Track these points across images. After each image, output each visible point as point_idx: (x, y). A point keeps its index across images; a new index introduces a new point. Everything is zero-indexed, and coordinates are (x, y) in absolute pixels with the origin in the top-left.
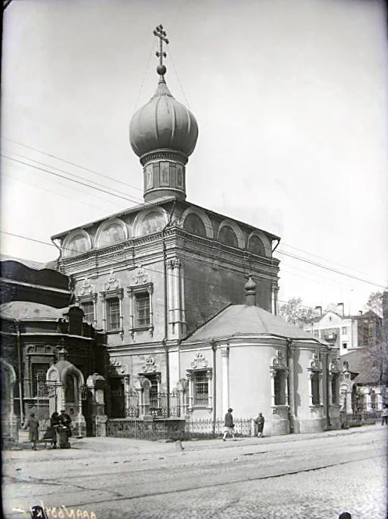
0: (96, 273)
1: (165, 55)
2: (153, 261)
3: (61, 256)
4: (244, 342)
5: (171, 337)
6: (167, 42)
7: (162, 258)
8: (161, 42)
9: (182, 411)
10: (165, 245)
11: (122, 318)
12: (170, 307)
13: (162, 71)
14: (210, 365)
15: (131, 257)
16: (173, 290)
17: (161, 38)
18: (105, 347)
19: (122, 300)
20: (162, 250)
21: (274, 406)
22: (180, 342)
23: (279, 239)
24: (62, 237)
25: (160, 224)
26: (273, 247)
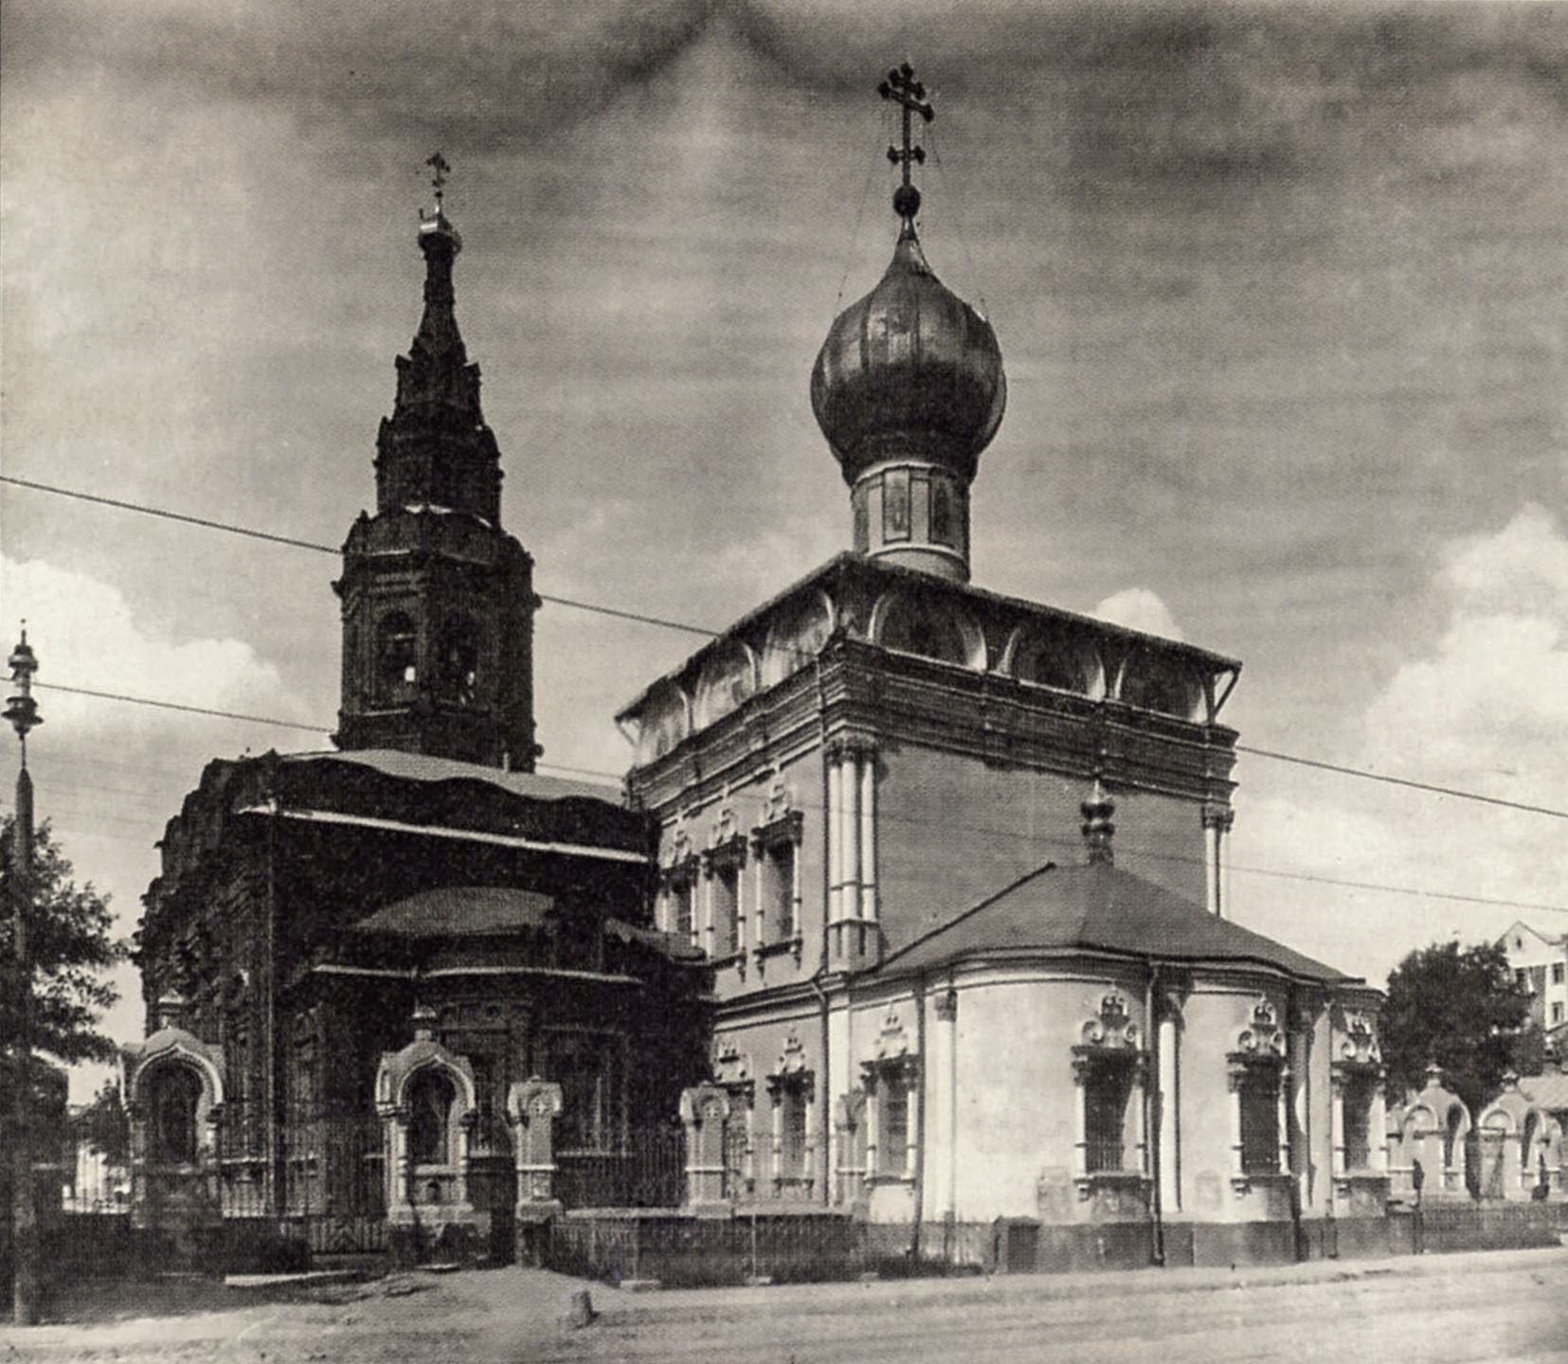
0: (695, 798)
1: (919, 155)
4: (1033, 967)
5: (833, 968)
6: (928, 114)
8: (906, 119)
9: (846, 1189)
11: (743, 919)
13: (907, 203)
14: (913, 1050)
15: (759, 745)
17: (908, 107)
18: (707, 1004)
23: (1235, 668)
24: (634, 712)
25: (819, 635)
26: (1218, 693)
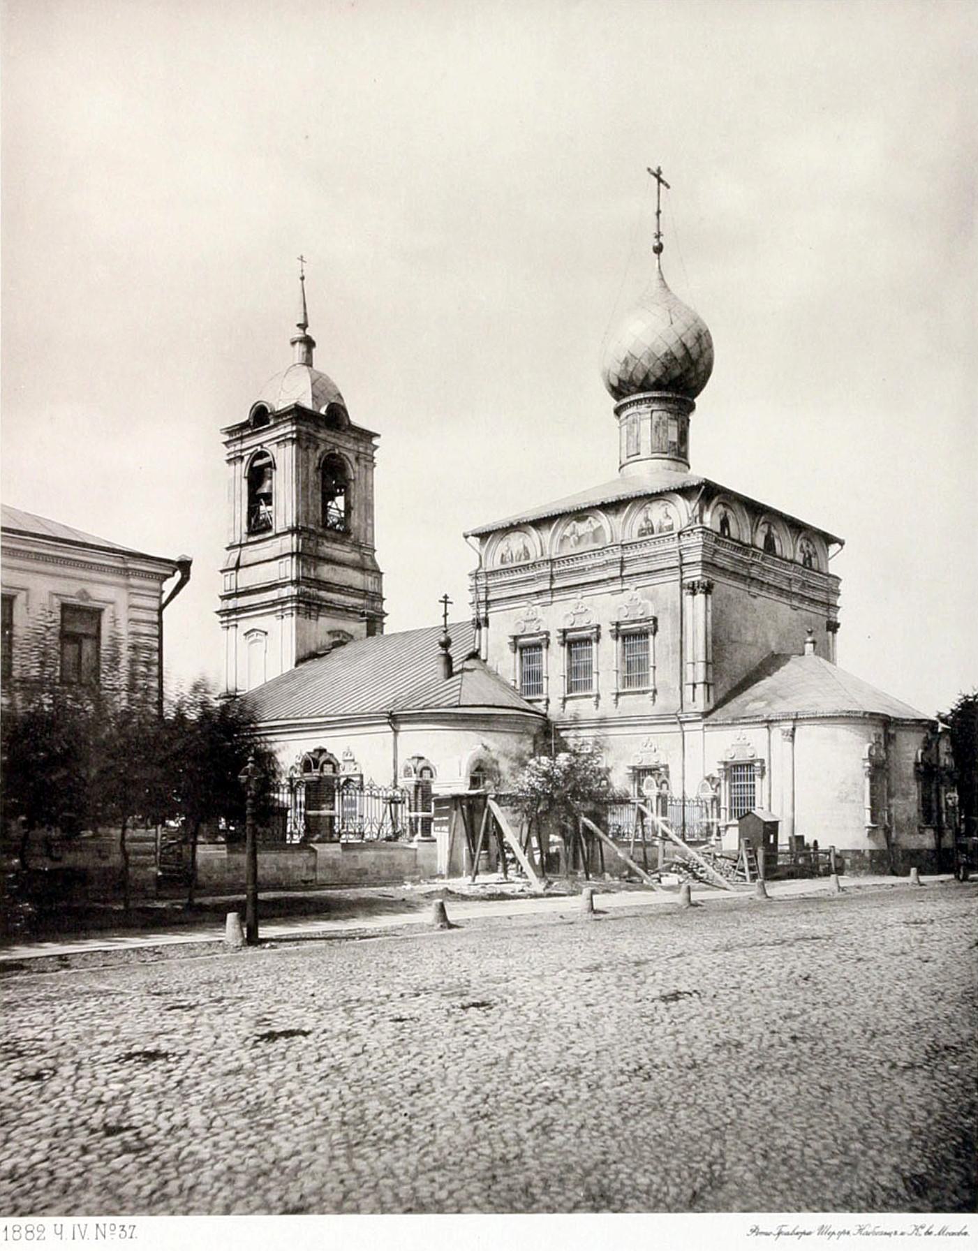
2: (582, 580)
3: (481, 566)
7: (678, 577)
10: (681, 555)
12: (689, 657)
16: (695, 632)
19: (654, 634)
20: (677, 564)
21: (871, 825)
22: (706, 714)
23: (842, 543)
24: (483, 536)
